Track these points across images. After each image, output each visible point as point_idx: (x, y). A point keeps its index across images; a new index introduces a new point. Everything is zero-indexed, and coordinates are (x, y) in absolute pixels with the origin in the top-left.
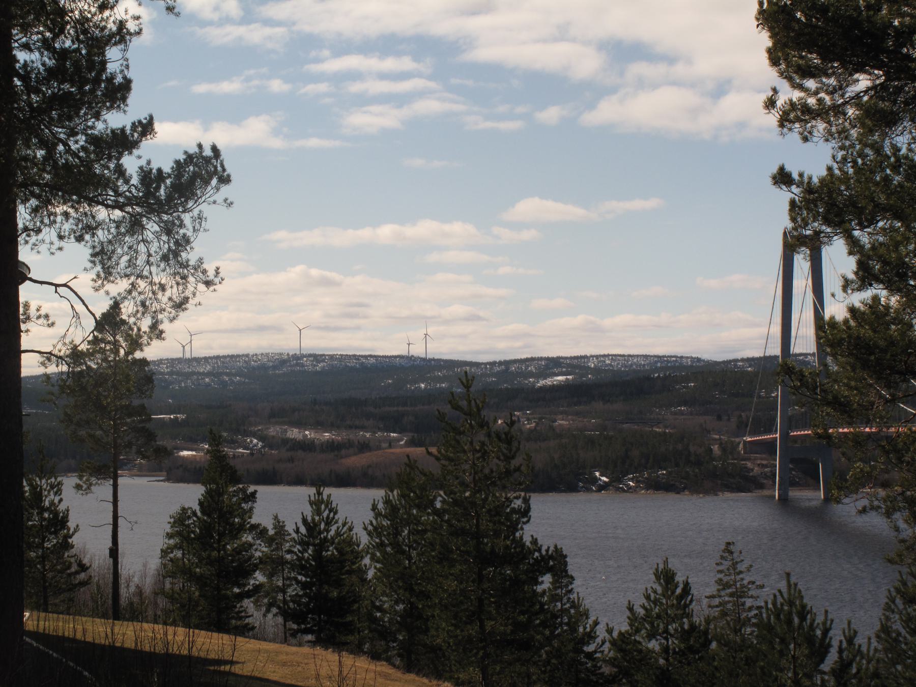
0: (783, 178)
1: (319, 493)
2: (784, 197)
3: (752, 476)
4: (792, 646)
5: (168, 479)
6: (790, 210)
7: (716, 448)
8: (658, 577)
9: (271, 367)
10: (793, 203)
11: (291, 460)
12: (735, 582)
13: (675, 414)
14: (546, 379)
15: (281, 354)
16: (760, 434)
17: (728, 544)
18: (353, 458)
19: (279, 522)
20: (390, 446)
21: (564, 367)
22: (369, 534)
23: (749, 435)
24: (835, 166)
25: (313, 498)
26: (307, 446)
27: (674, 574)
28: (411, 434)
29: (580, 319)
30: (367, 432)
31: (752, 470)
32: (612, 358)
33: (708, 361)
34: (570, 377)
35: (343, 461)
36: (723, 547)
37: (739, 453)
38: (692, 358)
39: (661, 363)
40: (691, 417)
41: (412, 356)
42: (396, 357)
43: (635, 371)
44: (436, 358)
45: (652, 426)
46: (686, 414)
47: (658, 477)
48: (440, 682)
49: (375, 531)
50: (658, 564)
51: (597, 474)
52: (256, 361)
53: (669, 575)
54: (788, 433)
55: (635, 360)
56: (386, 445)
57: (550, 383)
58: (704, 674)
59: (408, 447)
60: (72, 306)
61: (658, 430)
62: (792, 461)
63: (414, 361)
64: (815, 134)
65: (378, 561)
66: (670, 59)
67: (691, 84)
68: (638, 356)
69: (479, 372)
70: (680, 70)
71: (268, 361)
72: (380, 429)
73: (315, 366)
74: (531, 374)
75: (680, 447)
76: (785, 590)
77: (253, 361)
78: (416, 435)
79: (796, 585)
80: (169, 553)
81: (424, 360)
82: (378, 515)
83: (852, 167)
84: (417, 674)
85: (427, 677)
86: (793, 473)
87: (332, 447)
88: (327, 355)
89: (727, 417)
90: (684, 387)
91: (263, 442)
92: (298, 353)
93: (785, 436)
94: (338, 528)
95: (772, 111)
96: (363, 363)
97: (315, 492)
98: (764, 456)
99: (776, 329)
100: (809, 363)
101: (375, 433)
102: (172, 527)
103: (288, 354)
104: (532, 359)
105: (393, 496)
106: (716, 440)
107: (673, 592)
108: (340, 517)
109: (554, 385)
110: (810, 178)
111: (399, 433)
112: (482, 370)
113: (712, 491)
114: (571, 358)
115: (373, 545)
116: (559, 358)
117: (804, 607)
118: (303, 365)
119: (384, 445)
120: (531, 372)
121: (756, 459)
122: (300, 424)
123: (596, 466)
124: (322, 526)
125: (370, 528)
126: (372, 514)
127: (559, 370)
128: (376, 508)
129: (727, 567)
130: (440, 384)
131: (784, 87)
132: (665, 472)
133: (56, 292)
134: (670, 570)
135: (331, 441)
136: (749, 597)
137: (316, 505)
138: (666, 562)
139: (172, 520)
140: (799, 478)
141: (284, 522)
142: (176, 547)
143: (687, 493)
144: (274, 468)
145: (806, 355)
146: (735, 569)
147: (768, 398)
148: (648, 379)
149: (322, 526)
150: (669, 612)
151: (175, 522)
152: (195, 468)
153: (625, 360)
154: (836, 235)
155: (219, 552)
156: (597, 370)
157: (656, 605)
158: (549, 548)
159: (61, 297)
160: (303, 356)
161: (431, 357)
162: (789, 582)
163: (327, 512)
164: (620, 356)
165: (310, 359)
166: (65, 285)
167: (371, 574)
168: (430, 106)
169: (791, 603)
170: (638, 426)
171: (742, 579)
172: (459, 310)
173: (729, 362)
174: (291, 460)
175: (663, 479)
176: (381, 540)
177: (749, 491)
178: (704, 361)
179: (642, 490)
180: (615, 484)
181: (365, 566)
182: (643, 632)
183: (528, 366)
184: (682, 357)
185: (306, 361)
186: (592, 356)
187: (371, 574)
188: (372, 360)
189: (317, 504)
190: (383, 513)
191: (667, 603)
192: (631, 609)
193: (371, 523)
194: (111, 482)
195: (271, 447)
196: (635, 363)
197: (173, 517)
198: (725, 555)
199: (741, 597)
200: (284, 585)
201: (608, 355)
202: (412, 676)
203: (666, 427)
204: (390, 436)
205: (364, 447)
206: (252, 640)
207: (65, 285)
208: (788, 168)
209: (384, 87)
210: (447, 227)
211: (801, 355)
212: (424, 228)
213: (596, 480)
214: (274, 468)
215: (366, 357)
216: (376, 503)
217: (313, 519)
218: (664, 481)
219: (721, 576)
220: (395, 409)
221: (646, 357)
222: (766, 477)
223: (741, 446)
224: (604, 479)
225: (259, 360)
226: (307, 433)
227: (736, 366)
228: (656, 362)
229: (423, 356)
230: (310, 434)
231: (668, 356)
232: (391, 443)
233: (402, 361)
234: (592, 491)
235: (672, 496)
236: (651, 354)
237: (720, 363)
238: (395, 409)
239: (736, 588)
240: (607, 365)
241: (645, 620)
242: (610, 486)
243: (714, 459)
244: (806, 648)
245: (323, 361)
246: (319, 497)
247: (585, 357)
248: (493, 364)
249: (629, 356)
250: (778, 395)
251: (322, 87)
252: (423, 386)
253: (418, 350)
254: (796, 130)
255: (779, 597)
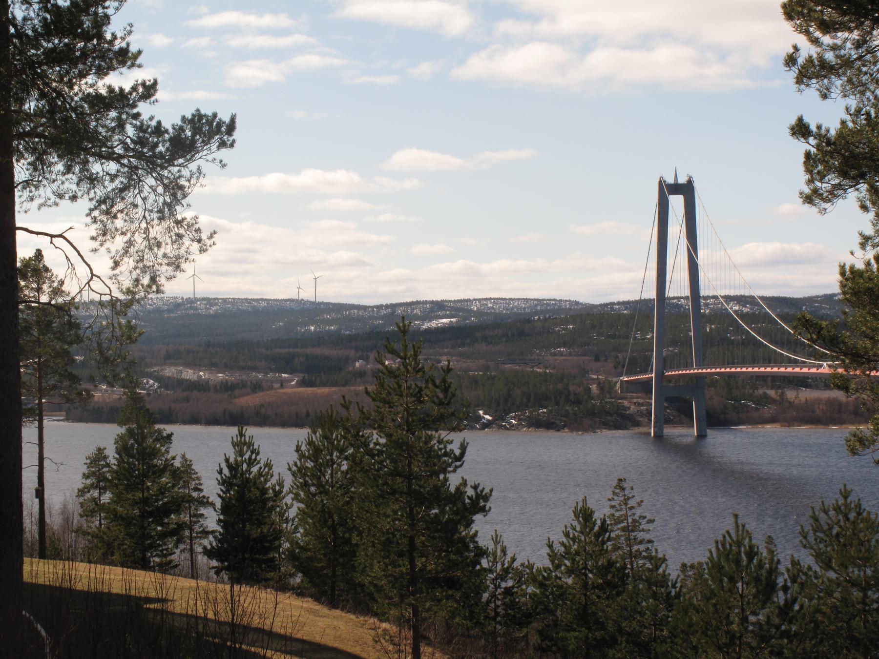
0: (801, 129)
1: (241, 434)
2: (801, 147)
3: (629, 414)
4: (740, 585)
5: (67, 419)
6: (805, 163)
7: (594, 388)
8: (576, 514)
9: (166, 310)
10: (808, 155)
11: (187, 400)
12: (626, 516)
13: (555, 354)
14: (431, 321)
15: (176, 298)
16: (636, 373)
17: (620, 480)
18: (247, 398)
19: (186, 461)
20: (282, 386)
21: (448, 310)
22: (294, 474)
23: (625, 375)
24: (848, 118)
25: (235, 439)
26: (200, 386)
27: (592, 512)
28: (302, 375)
29: (459, 264)
30: (259, 373)
31: (629, 408)
32: (494, 302)
33: (586, 304)
34: (454, 320)
35: (237, 400)
36: (615, 483)
37: (616, 392)
38: (570, 301)
39: (541, 306)
40: (570, 358)
41: (302, 300)
42: (286, 300)
43: (515, 314)
44: (325, 301)
45: (533, 367)
46: (565, 355)
47: (539, 415)
48: (366, 618)
49: (299, 472)
50: (577, 503)
51: (481, 412)
52: (151, 305)
53: (588, 513)
54: (663, 373)
55: (516, 304)
56: (279, 385)
57: (434, 326)
58: (626, 609)
59: (299, 387)
60: (67, 257)
61: (538, 370)
62: (667, 399)
63: (304, 304)
64: (832, 90)
65: (301, 501)
66: (535, 17)
67: (562, 40)
68: (518, 299)
69: (366, 315)
70: (544, 27)
71: (163, 305)
72: (272, 370)
73: (208, 309)
74: (417, 317)
75: (560, 386)
76: (733, 533)
77: (149, 304)
78: (306, 375)
79: (744, 526)
80: (86, 493)
81: (314, 303)
82: (302, 456)
83: (866, 119)
84: (342, 610)
85: (354, 613)
86: (668, 411)
87: (227, 387)
88: (221, 299)
89: (604, 358)
90: (564, 329)
91: (159, 383)
92: (192, 296)
93: (660, 376)
94: (260, 468)
95: (793, 68)
96: (255, 306)
97: (237, 433)
98: (640, 395)
99: (653, 274)
100: (681, 306)
101: (267, 373)
102: (88, 467)
103: (182, 298)
104: (418, 303)
105: (316, 437)
106: (593, 379)
107: (592, 529)
108: (262, 458)
109: (438, 327)
110: (828, 131)
111: (291, 374)
112: (369, 312)
113: (591, 428)
114: (455, 301)
115: (297, 486)
116: (443, 301)
117: (751, 547)
118: (196, 309)
119: (276, 385)
120: (416, 315)
121: (632, 398)
122: (195, 365)
123: (480, 405)
124: (245, 466)
125: (294, 468)
126: (296, 455)
127: (444, 312)
128: (300, 450)
129: (619, 502)
130: (329, 326)
131: (802, 41)
132: (545, 410)
133: (51, 242)
134: (589, 508)
135: (224, 381)
136: (640, 531)
137: (238, 446)
138: (585, 500)
139: (88, 461)
140: (673, 416)
141: (191, 461)
142: (92, 486)
143: (567, 430)
144: (170, 408)
145: (679, 298)
146: (626, 504)
147: (643, 339)
148: (529, 321)
149: (245, 466)
150: (587, 548)
151: (91, 463)
152: (94, 408)
153: (506, 303)
154: (850, 188)
155: (143, 492)
156: (479, 313)
157: (574, 541)
158: (483, 489)
159: (56, 248)
160: (197, 300)
161: (320, 301)
162: (736, 523)
163: (249, 453)
164: (502, 299)
165: (204, 302)
166: (61, 236)
167: (292, 513)
168: (313, 60)
169: (739, 544)
170: (520, 366)
171: (634, 514)
172: (344, 255)
173: (606, 305)
174: (187, 400)
175: (543, 417)
176: (304, 480)
177: (626, 428)
178: (581, 304)
179: (524, 427)
180: (498, 422)
181: (286, 504)
182: (563, 568)
183: (414, 309)
184: (561, 301)
185: (200, 305)
186: (475, 300)
187: (292, 513)
188: (264, 304)
189: (241, 445)
190: (307, 454)
191: (585, 540)
192: (550, 546)
193: (296, 465)
194: (36, 423)
195: (167, 388)
196: (516, 306)
197: (89, 458)
198: (617, 491)
199: (633, 531)
200: (191, 521)
201: (490, 299)
202: (338, 612)
203: (546, 368)
204: (281, 376)
205: (257, 387)
206: (180, 578)
207: (61, 236)
208: (806, 119)
209: (262, 41)
210: (330, 176)
211: (674, 298)
212: (309, 177)
213: (480, 418)
214: (170, 408)
215: (257, 300)
216: (300, 444)
217: (236, 460)
218: (545, 418)
219: (613, 511)
220: (287, 350)
221: (526, 300)
222: (642, 415)
223: (618, 385)
224: (488, 417)
225: (155, 304)
226: (201, 373)
227: (612, 308)
228: (536, 305)
229: (313, 299)
230: (205, 375)
231: (548, 300)
232: (283, 383)
233: (292, 304)
234: (476, 428)
235: (552, 433)
236: (532, 297)
237: (597, 306)
238: (287, 350)
239: (628, 523)
240: (489, 308)
241: (564, 557)
242: (493, 424)
243: (592, 398)
244: (754, 587)
245: (216, 304)
246: (241, 438)
247: (468, 300)
248: (380, 307)
249: (511, 299)
250: (653, 337)
251: (204, 41)
252: (312, 328)
253: (307, 295)
254: (813, 86)
255: (728, 538)
